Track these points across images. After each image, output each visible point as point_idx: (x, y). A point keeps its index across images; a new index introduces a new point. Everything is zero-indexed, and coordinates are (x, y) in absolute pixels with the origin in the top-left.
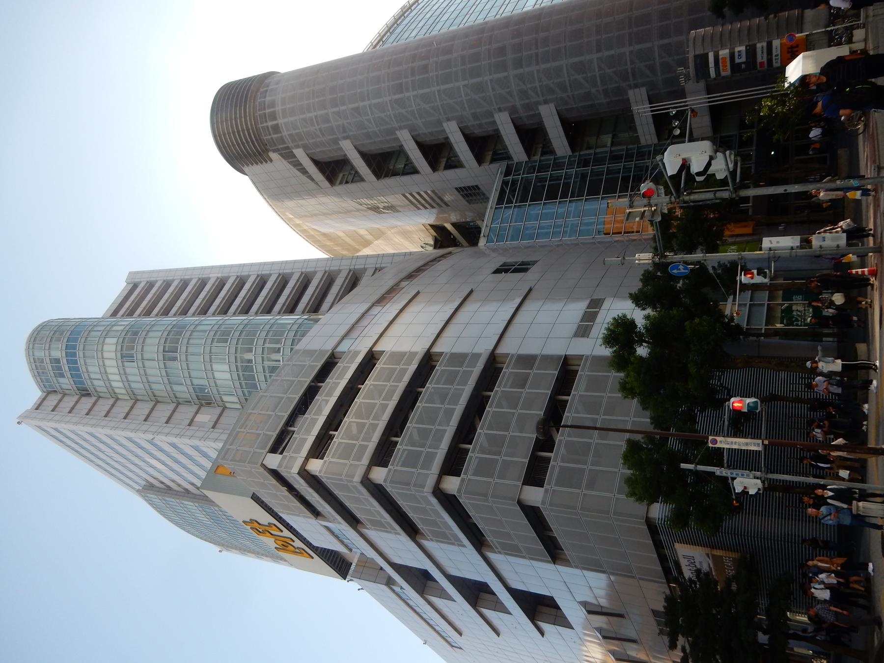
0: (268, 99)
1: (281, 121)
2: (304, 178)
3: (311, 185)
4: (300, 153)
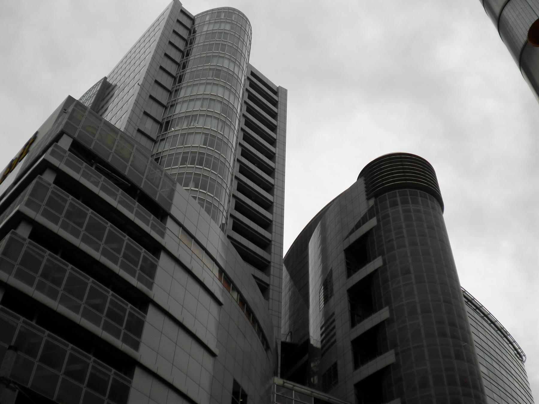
0: (420, 199)
1: (400, 208)
2: (352, 225)
3: (346, 233)
4: (373, 222)
